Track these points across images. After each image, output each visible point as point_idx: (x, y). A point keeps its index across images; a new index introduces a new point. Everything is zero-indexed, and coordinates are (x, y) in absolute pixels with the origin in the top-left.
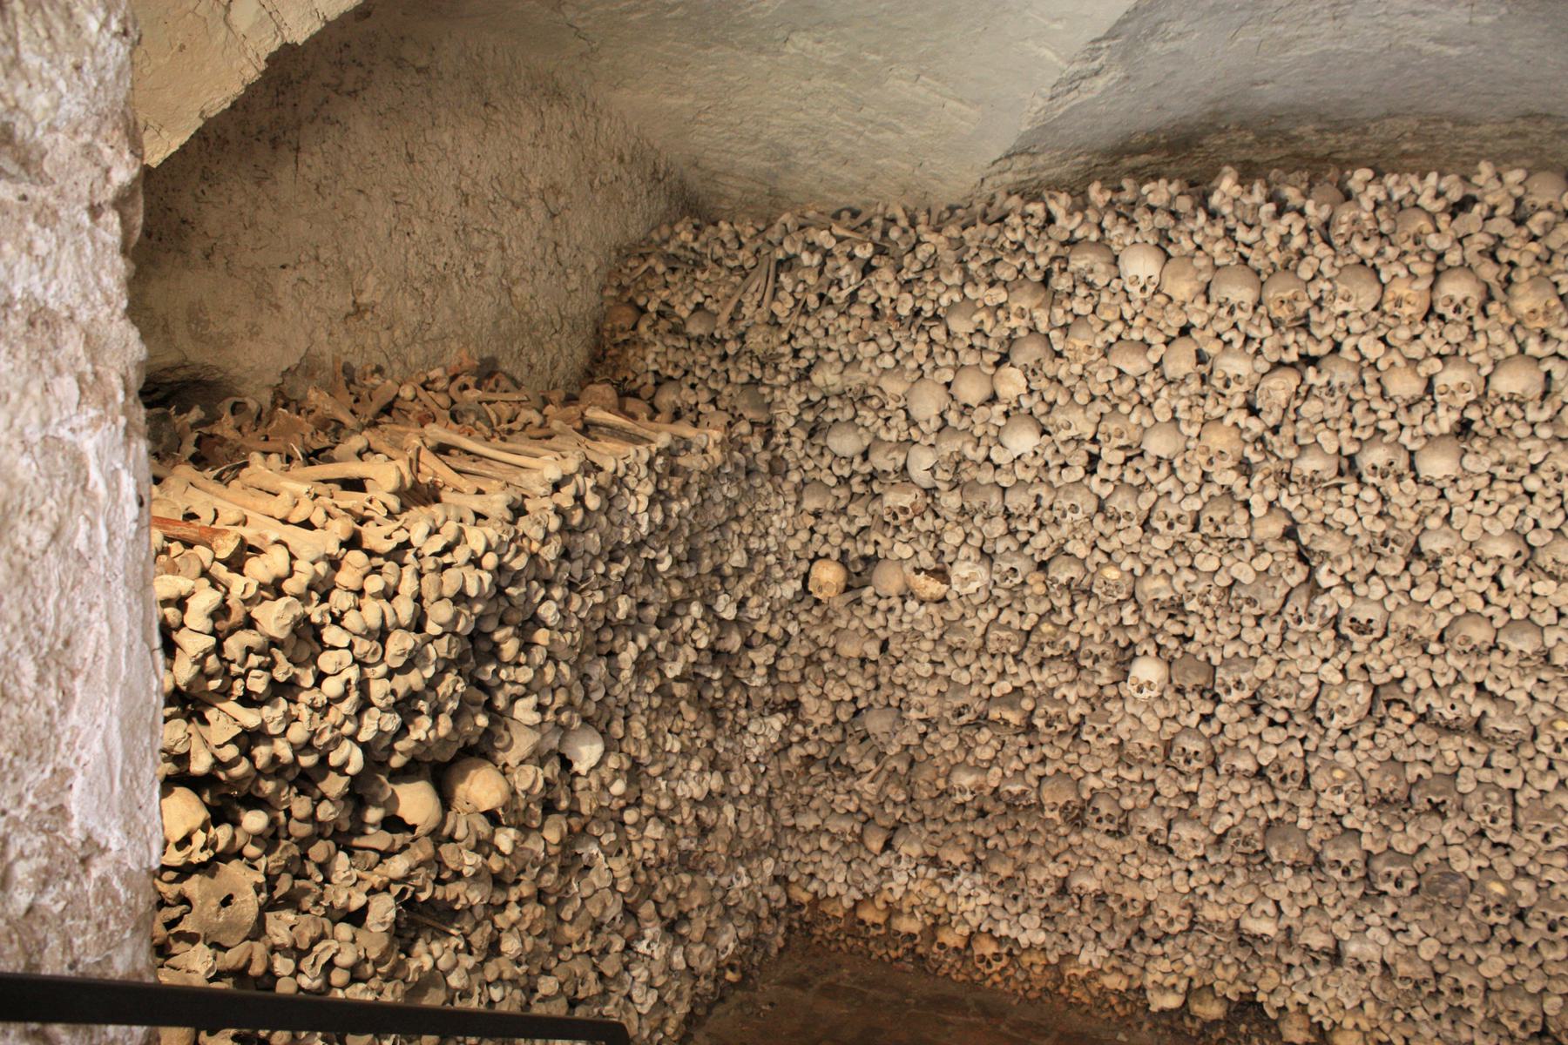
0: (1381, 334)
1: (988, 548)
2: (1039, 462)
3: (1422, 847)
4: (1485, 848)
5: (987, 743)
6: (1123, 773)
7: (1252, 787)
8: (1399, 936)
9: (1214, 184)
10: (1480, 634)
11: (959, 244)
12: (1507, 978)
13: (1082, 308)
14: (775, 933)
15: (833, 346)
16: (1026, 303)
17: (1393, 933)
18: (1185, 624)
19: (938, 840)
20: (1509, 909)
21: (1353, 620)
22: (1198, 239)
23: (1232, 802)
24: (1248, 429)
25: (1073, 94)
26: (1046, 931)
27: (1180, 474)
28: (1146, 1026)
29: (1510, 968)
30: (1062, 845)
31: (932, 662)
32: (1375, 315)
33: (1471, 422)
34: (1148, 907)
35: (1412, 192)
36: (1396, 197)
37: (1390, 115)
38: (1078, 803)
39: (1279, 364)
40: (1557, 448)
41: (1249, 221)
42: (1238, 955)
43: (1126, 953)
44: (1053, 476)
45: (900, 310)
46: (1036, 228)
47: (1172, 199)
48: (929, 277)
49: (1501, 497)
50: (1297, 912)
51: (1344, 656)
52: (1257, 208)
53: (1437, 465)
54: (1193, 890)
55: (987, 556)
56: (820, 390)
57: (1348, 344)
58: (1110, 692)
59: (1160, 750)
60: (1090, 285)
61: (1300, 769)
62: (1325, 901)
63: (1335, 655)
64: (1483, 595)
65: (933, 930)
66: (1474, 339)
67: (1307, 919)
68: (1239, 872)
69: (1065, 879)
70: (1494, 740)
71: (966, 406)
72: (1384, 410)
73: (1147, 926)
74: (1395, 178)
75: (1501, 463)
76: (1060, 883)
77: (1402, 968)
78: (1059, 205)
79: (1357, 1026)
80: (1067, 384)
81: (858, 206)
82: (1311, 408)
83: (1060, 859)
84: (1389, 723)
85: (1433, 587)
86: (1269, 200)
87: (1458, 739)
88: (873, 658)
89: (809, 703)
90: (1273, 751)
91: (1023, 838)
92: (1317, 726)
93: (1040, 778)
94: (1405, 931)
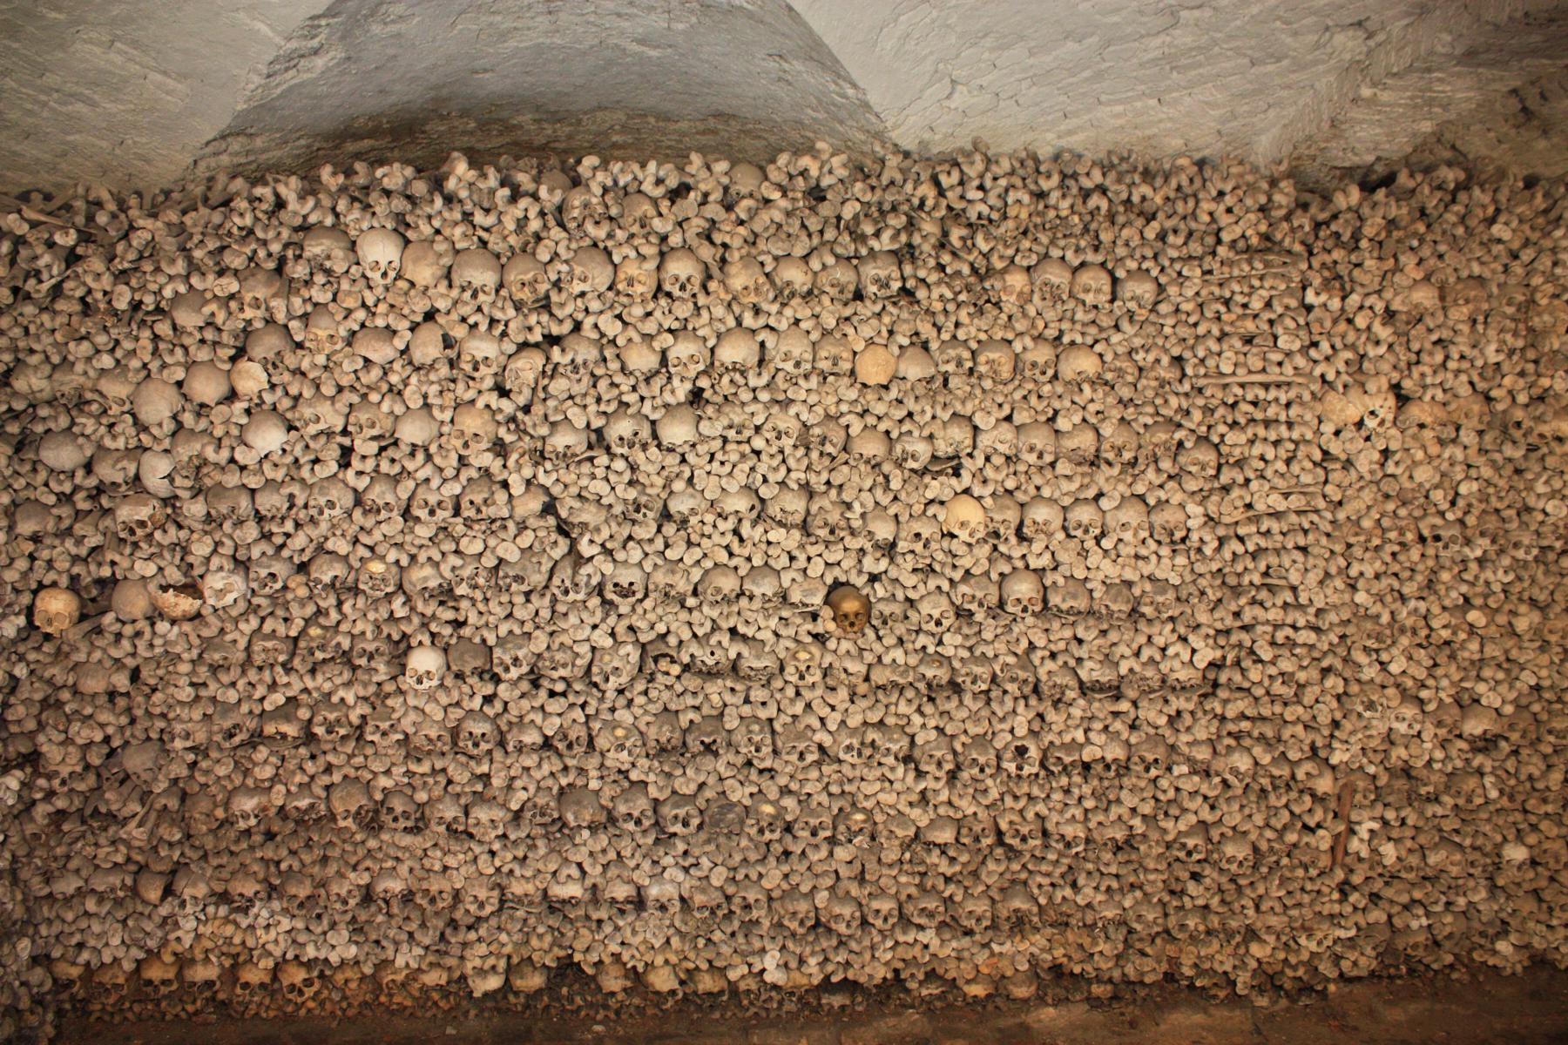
1: (241, 555)
2: (289, 459)
3: (702, 786)
4: (754, 776)
5: (266, 761)
6: (414, 767)
7: (541, 759)
8: (692, 871)
9: (445, 169)
10: (728, 584)
11: (180, 230)
12: (785, 886)
13: (322, 296)
14: (43, 1023)
15: (36, 347)
16: (261, 293)
17: (686, 870)
18: (457, 609)
19: (225, 874)
20: (780, 824)
21: (616, 585)
22: (437, 223)
23: (525, 777)
24: (500, 410)
25: (292, 73)
26: (357, 943)
27: (438, 460)
28: (472, 1013)
29: (786, 876)
30: (361, 852)
31: (192, 684)
32: (610, 294)
33: (702, 390)
34: (457, 896)
35: (635, 178)
36: (621, 183)
37: (600, 108)
38: (371, 806)
39: (524, 346)
41: (486, 205)
42: (551, 923)
43: (442, 947)
44: (305, 472)
45: (115, 304)
46: (266, 212)
47: (408, 183)
48: (148, 267)
50: (599, 869)
51: (612, 620)
52: (492, 192)
53: (677, 432)
54: (498, 870)
55: (242, 564)
56: (25, 397)
57: (588, 323)
58: (389, 688)
59: (447, 738)
60: (328, 272)
61: (583, 734)
64: (727, 547)
65: (231, 974)
66: (699, 315)
67: (609, 874)
68: (541, 843)
69: (368, 886)
70: (749, 678)
71: (202, 405)
72: (625, 384)
73: (458, 915)
74: (620, 164)
75: (731, 427)
76: (364, 891)
77: (699, 899)
78: (289, 189)
79: (667, 962)
80: (311, 376)
81: (49, 188)
82: (559, 386)
83: (361, 867)
84: (660, 677)
85: (684, 546)
86: (502, 185)
87: (720, 682)
88: (123, 690)
89: (52, 752)
90: (557, 721)
91: (318, 853)
93: (327, 788)
94: (696, 865)
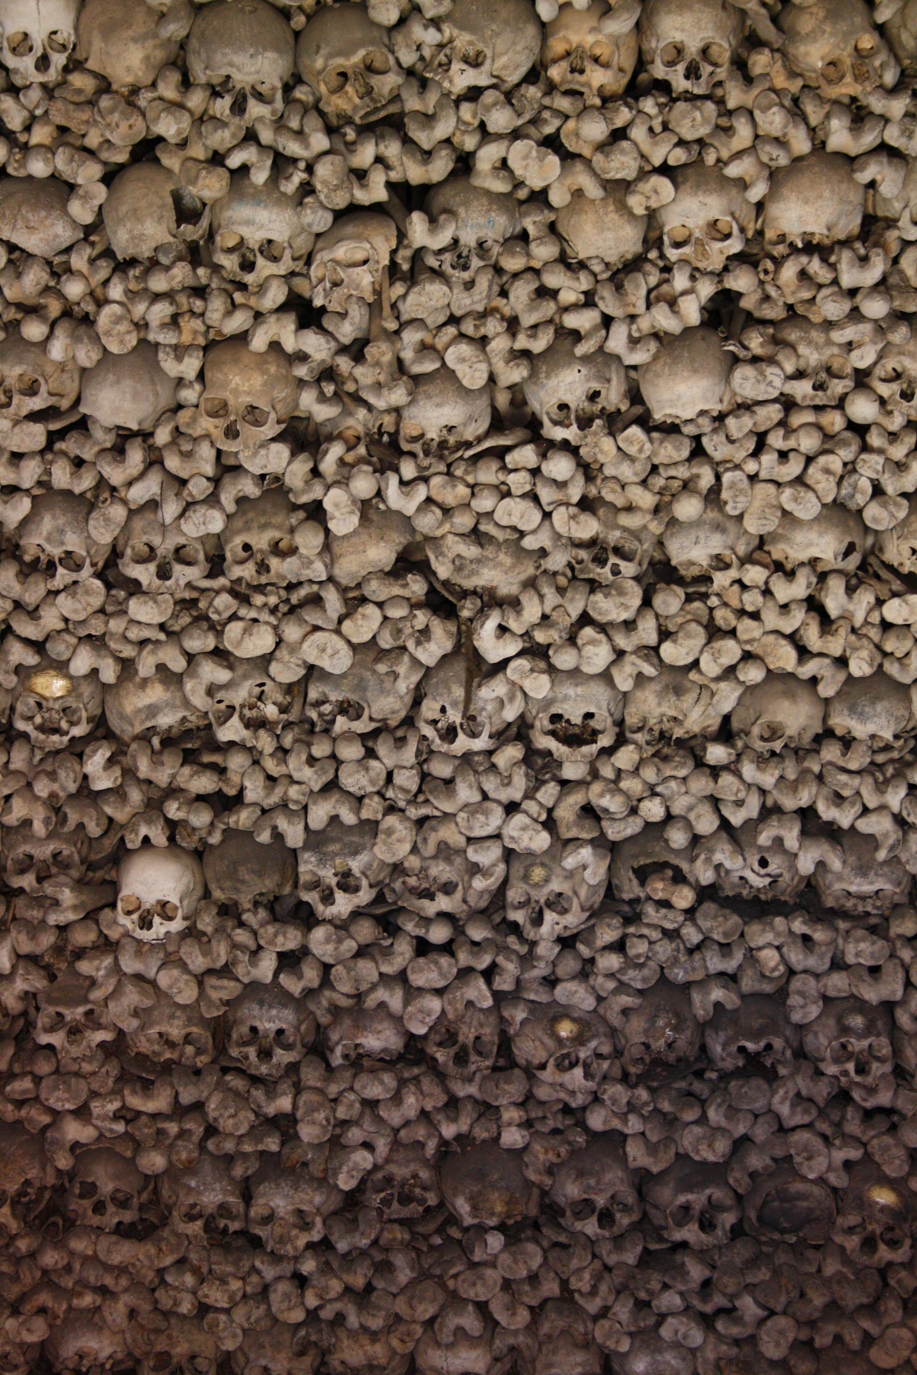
0: (549, 130)
4: (853, 1126)
6: (136, 1102)
7: (402, 1083)
17: (707, 1321)
21: (556, 718)
23: (367, 1124)
24: (302, 357)
27: (173, 463)
30: (29, 1277)
40: (900, 334)
49: (808, 442)
50: (523, 1316)
51: (548, 793)
57: (488, 156)
61: (489, 1033)
62: (574, 1284)
63: (529, 795)
64: (793, 638)
67: (545, 1328)
68: (399, 1260)
83: (28, 1308)
85: (699, 635)
87: (779, 921)
92: (512, 941)
